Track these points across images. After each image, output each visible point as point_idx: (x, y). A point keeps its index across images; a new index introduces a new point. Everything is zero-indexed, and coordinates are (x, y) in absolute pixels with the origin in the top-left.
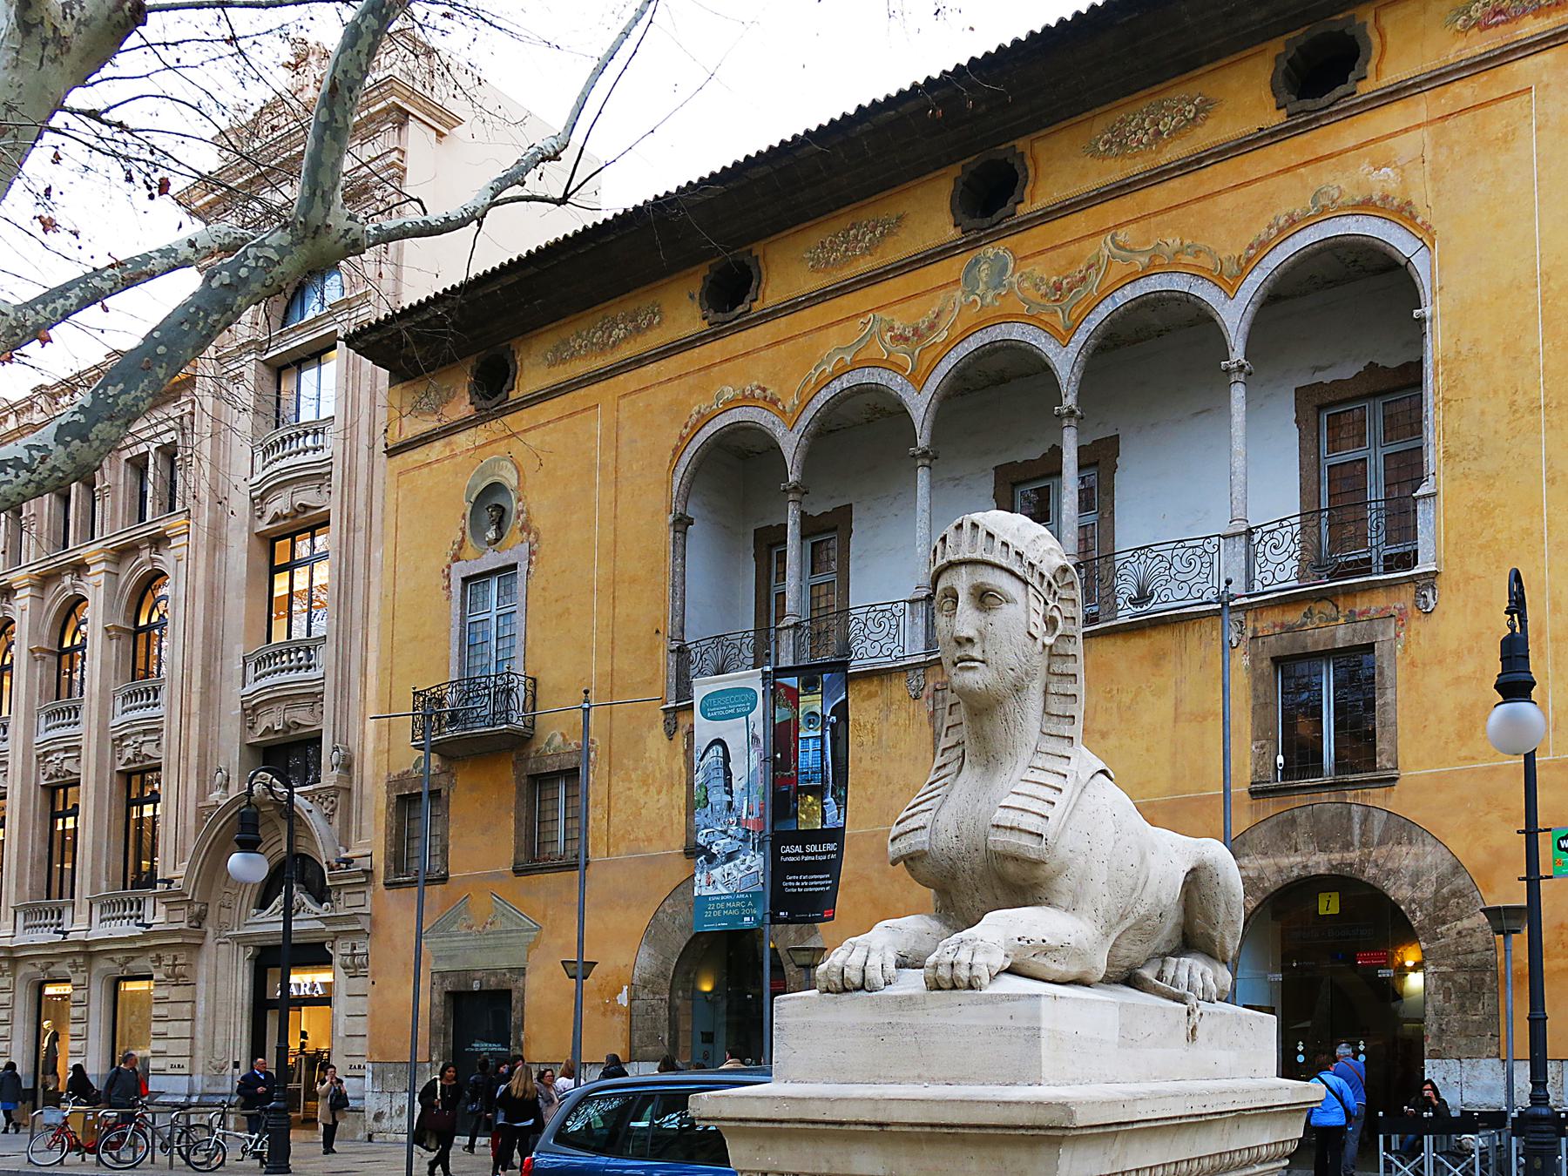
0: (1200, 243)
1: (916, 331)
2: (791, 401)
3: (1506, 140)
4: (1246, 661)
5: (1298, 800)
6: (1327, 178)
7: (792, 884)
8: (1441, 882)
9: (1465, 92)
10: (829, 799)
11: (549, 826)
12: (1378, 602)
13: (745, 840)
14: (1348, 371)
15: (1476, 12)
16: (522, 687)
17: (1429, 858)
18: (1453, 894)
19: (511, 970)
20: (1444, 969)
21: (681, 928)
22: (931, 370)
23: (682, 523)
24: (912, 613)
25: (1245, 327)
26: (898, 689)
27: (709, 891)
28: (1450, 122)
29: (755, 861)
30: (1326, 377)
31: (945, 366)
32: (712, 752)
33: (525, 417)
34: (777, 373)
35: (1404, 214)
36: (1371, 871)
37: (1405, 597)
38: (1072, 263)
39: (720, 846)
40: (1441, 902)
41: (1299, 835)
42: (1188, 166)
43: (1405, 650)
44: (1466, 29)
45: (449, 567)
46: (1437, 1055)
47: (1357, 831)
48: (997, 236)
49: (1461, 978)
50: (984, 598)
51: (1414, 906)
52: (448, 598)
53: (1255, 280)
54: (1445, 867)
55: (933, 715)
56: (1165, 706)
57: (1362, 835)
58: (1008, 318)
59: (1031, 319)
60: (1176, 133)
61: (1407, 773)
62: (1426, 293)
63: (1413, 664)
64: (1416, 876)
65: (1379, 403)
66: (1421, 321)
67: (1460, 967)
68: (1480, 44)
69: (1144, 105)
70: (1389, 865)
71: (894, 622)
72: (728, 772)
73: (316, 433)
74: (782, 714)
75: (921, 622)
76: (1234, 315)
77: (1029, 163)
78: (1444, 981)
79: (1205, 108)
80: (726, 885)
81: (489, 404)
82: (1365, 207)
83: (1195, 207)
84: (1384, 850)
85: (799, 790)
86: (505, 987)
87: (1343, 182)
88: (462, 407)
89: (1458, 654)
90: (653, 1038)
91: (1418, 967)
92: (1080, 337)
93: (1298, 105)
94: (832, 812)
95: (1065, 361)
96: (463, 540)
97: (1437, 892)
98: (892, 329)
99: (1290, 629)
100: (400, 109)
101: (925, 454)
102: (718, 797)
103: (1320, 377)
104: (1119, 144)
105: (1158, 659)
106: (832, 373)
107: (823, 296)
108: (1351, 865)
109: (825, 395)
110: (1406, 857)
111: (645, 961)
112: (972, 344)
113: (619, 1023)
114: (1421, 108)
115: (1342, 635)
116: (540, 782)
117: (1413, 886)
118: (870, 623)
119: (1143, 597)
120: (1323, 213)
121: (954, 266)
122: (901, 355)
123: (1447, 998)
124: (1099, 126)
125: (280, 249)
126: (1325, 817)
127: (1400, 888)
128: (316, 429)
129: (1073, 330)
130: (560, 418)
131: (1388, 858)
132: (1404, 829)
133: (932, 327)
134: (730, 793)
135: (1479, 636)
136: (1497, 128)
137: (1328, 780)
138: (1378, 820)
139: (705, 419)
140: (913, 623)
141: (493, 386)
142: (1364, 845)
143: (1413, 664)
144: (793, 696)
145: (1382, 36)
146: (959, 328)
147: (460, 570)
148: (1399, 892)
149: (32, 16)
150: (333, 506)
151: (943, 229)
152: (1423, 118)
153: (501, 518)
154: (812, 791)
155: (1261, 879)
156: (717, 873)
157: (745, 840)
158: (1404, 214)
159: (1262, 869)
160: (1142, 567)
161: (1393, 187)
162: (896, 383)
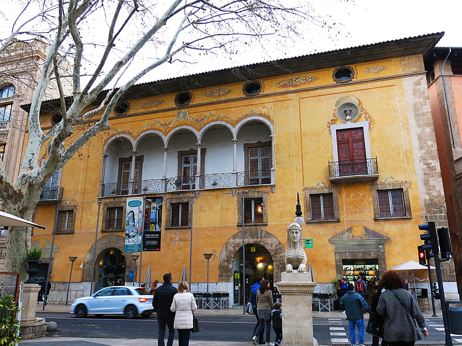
0: (228, 116)
1: (165, 124)
2: (135, 134)
3: (287, 108)
4: (236, 199)
5: (247, 228)
6: (253, 108)
7: (148, 243)
8: (276, 246)
9: (280, 98)
10: (157, 225)
11: (63, 223)
12: (264, 189)
13: (137, 233)
14: (254, 142)
15: (281, 84)
18: (279, 248)
21: (99, 249)
23: (105, 157)
25: (237, 133)
27: (129, 244)
28: (277, 102)
29: (140, 238)
30: (250, 142)
31: (172, 132)
32: (130, 214)
34: (133, 128)
35: (268, 117)
36: (262, 243)
37: (269, 189)
38: (201, 116)
39: (131, 234)
40: (276, 250)
41: (247, 235)
42: (226, 101)
44: (279, 87)
48: (185, 108)
49: (281, 266)
50: (296, 233)
53: (239, 125)
54: (277, 243)
56: (219, 206)
58: (187, 124)
59: (191, 125)
60: (223, 95)
61: (269, 224)
62: (272, 133)
63: (270, 202)
64: (272, 244)
65: (260, 149)
66: (272, 137)
67: (281, 263)
68: (282, 90)
69: (217, 89)
72: (134, 218)
74: (147, 207)
75: (164, 184)
76: (235, 131)
77: (192, 95)
79: (229, 92)
80: (133, 243)
82: (261, 115)
83: (227, 109)
84: (265, 239)
85: (150, 223)
87: (257, 110)
89: (279, 201)
90: (89, 276)
91: (261, 261)
92: (202, 130)
93: (248, 94)
94: (158, 228)
95: (199, 135)
99: (246, 193)
100: (38, 56)
101: (166, 149)
102: (131, 223)
103: (248, 142)
104: (212, 95)
105: (217, 197)
107: (144, 114)
109: (143, 134)
110: (269, 241)
111: (88, 257)
112: (178, 128)
113: (80, 272)
114: (271, 99)
115: (256, 195)
116: (62, 212)
119: (215, 184)
120: (252, 115)
121: (175, 112)
122: (162, 128)
123: (278, 270)
124: (208, 91)
125: (97, 129)
126: (253, 231)
129: (201, 129)
132: (269, 235)
133: (169, 124)
134: (134, 223)
135: (283, 198)
136: (285, 105)
137: (254, 224)
138: (264, 233)
140: (162, 184)
142: (261, 238)
143: (270, 202)
144: (150, 203)
145: (264, 85)
146: (176, 125)
148: (268, 248)
149: (82, 100)
150: (7, 141)
151: (172, 104)
152: (272, 101)
154: (153, 223)
155: (239, 244)
156: (130, 240)
157: (137, 233)
158: (268, 117)
159: (239, 242)
161: (266, 112)
162: (160, 134)
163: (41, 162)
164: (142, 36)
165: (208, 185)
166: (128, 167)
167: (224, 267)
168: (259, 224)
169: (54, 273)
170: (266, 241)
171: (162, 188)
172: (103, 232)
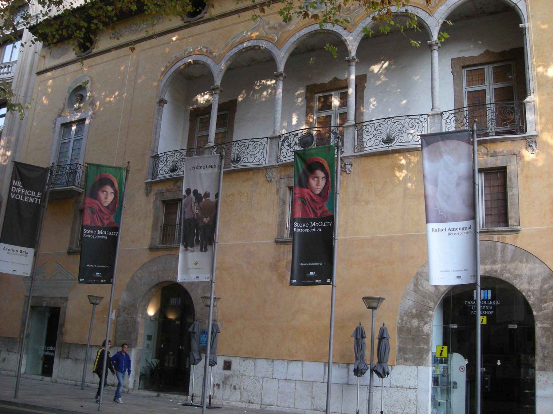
16: (81, 170)
17: (537, 270)
19: (61, 298)
20: (545, 325)
22: (286, 40)
24: (270, 143)
26: (261, 178)
33: (98, 59)
43: (522, 170)
45: (56, 119)
46: (543, 369)
47: (499, 254)
51: (529, 293)
52: (54, 132)
55: (278, 190)
57: (502, 257)
63: (527, 177)
70: (516, 272)
71: (262, 147)
73: (9, 66)
78: (546, 331)
81: (83, 54)
86: (58, 306)
88: (71, 55)
96: (64, 108)
97: (541, 287)
98: (268, 24)
106: (239, 42)
108: (496, 271)
109: (236, 50)
117: (529, 283)
118: (250, 147)
127: (522, 284)
128: (9, 65)
130: (113, 60)
131: (516, 269)
132: (526, 255)
138: (510, 248)
139: (178, 60)
141: (86, 48)
143: (527, 177)
147: (61, 121)
153: (81, 98)
160: (389, 126)
163: (55, 124)
164: (241, 14)
165: (372, 144)
166: (206, 125)
167: (409, 331)
168: (496, 229)
169: (68, 326)
170: (516, 269)
171: (270, 156)
172: (152, 249)
